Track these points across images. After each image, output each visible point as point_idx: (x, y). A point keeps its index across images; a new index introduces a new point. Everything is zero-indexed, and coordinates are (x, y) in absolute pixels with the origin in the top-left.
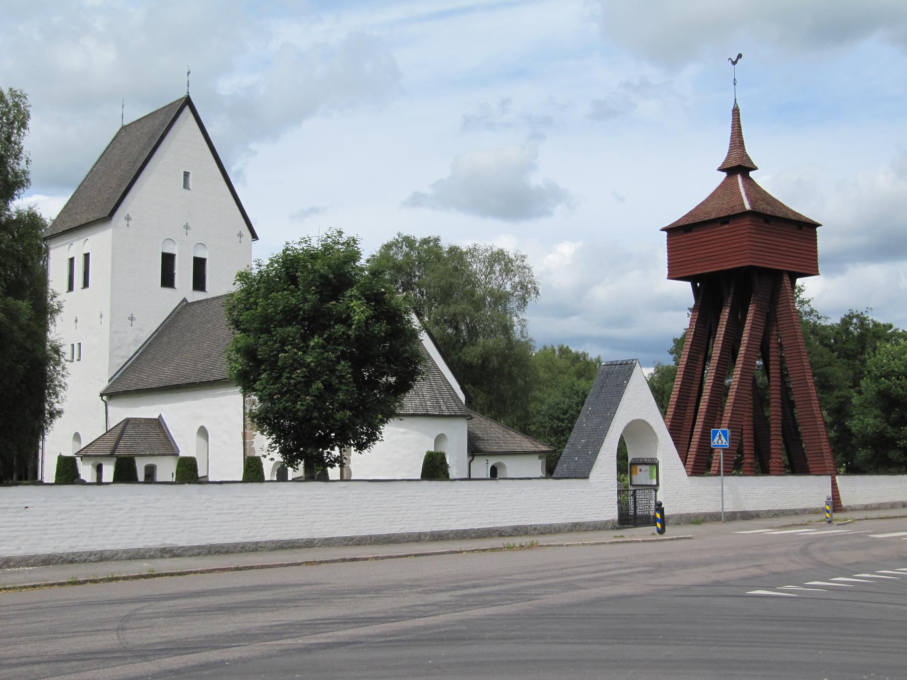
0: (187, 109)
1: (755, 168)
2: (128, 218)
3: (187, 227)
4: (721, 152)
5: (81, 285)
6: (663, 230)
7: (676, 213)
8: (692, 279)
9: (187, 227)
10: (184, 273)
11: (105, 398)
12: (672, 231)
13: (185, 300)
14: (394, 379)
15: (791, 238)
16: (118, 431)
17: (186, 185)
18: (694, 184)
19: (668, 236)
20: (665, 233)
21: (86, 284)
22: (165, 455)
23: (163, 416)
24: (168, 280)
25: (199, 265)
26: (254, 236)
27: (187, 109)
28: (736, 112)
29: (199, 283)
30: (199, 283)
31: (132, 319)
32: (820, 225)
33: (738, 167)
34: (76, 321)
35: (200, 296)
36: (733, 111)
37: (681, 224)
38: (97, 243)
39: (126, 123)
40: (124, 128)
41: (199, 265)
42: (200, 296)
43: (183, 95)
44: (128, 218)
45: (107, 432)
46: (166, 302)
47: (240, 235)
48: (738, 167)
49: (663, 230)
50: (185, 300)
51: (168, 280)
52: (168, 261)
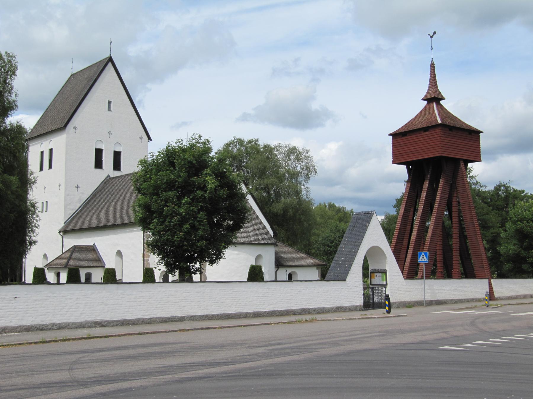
0: (110, 64)
1: (443, 99)
2: (75, 128)
3: (110, 133)
4: (424, 89)
5: (48, 167)
6: (390, 135)
7: (397, 125)
8: (407, 164)
9: (110, 133)
10: (108, 160)
11: (61, 233)
12: (395, 135)
13: (108, 176)
14: (232, 222)
15: (465, 139)
16: (70, 253)
17: (109, 109)
18: (408, 108)
19: (393, 139)
20: (391, 137)
21: (50, 167)
22: (97, 267)
23: (96, 244)
24: (99, 164)
25: (117, 155)
26: (150, 139)
27: (110, 64)
28: (432, 66)
29: (117, 166)
30: (117, 166)
31: (77, 187)
32: (482, 132)
33: (434, 98)
34: (45, 188)
35: (117, 174)
36: (431, 65)
37: (400, 131)
38: (57, 143)
39: (74, 72)
40: (73, 75)
41: (117, 155)
42: (117, 174)
43: (108, 55)
44: (75, 128)
45: (63, 253)
46: (98, 177)
47: (141, 138)
48: (434, 98)
49: (390, 135)
50: (108, 176)
51: (99, 164)
52: (99, 153)
